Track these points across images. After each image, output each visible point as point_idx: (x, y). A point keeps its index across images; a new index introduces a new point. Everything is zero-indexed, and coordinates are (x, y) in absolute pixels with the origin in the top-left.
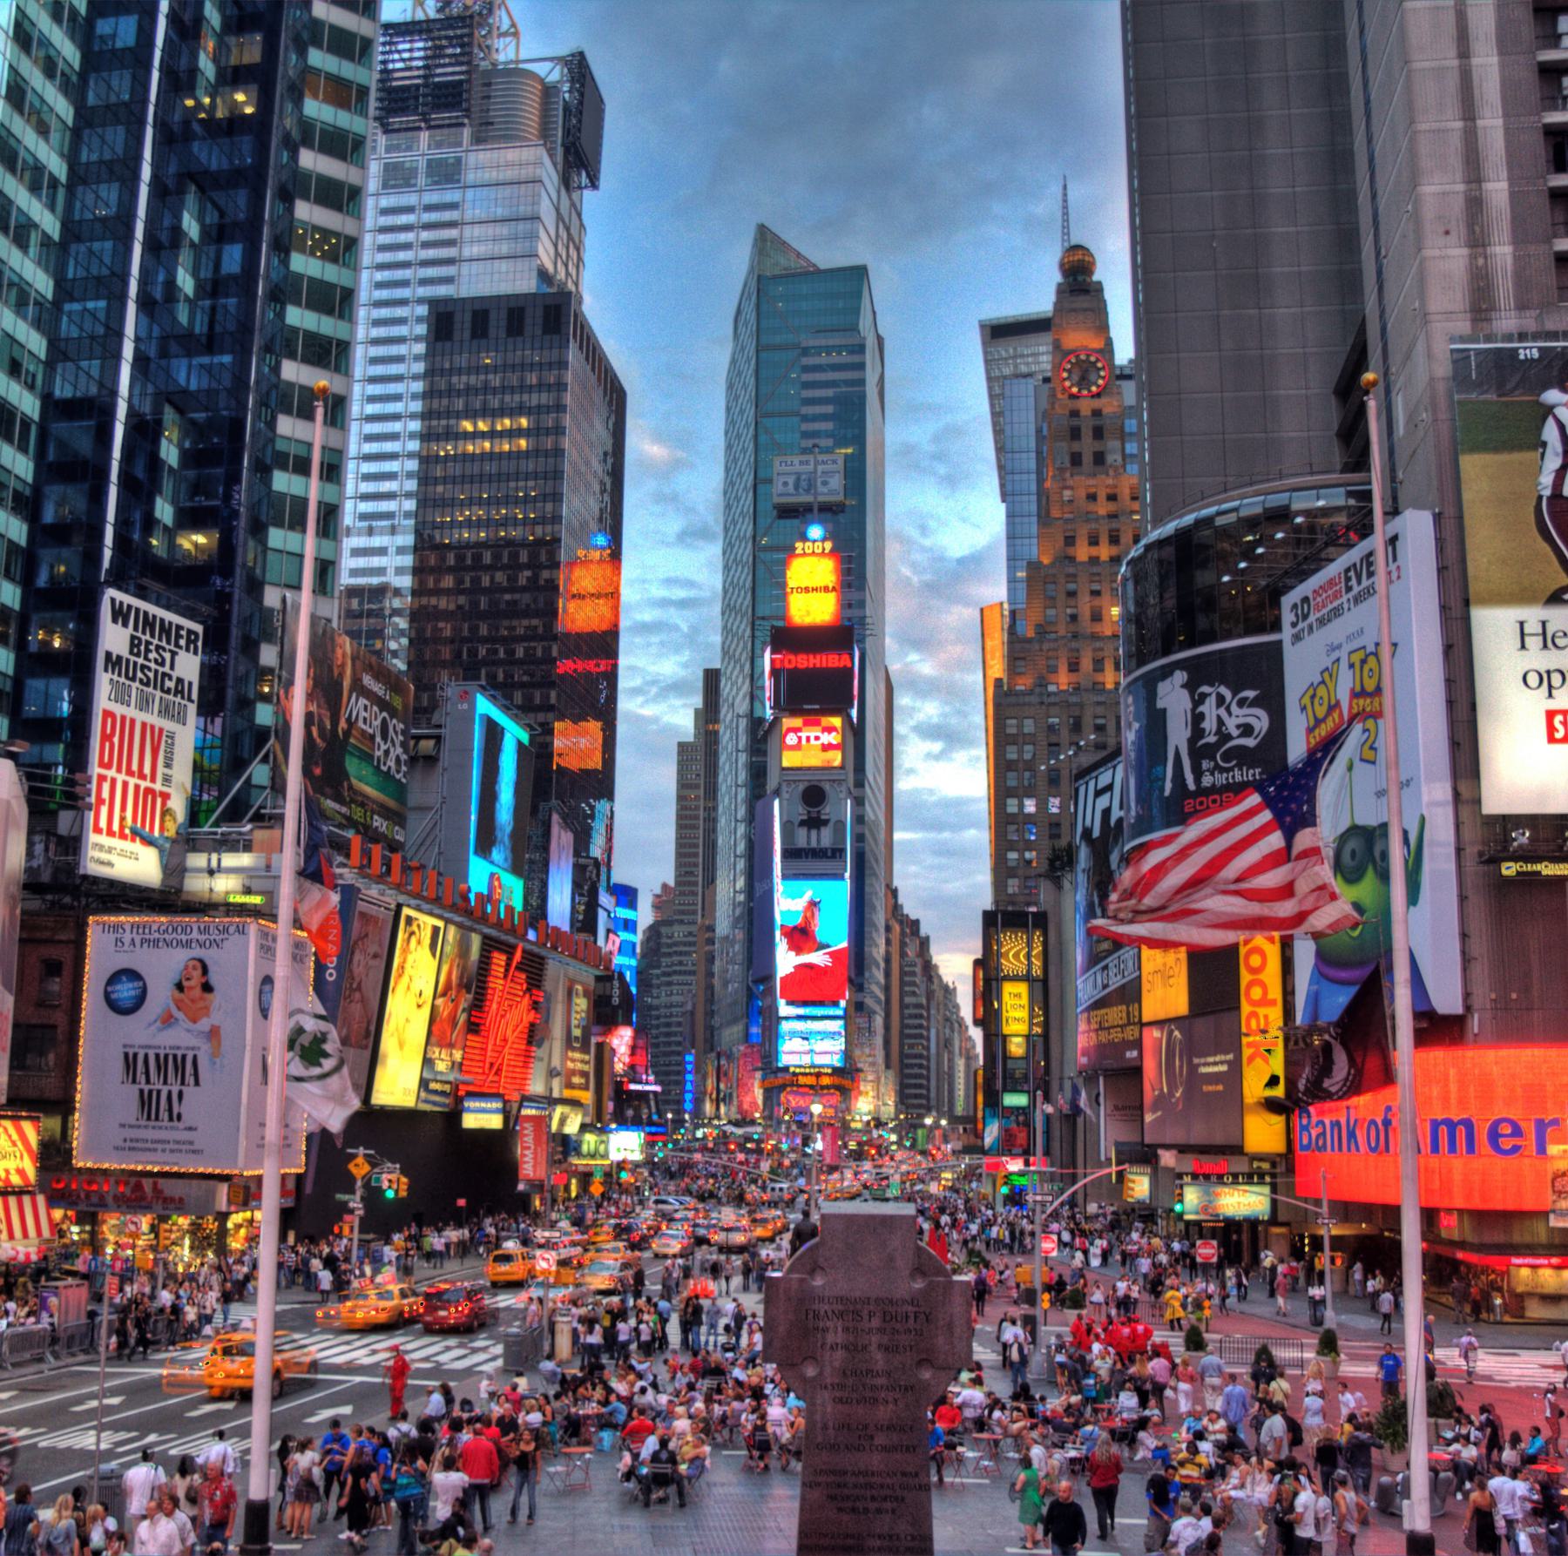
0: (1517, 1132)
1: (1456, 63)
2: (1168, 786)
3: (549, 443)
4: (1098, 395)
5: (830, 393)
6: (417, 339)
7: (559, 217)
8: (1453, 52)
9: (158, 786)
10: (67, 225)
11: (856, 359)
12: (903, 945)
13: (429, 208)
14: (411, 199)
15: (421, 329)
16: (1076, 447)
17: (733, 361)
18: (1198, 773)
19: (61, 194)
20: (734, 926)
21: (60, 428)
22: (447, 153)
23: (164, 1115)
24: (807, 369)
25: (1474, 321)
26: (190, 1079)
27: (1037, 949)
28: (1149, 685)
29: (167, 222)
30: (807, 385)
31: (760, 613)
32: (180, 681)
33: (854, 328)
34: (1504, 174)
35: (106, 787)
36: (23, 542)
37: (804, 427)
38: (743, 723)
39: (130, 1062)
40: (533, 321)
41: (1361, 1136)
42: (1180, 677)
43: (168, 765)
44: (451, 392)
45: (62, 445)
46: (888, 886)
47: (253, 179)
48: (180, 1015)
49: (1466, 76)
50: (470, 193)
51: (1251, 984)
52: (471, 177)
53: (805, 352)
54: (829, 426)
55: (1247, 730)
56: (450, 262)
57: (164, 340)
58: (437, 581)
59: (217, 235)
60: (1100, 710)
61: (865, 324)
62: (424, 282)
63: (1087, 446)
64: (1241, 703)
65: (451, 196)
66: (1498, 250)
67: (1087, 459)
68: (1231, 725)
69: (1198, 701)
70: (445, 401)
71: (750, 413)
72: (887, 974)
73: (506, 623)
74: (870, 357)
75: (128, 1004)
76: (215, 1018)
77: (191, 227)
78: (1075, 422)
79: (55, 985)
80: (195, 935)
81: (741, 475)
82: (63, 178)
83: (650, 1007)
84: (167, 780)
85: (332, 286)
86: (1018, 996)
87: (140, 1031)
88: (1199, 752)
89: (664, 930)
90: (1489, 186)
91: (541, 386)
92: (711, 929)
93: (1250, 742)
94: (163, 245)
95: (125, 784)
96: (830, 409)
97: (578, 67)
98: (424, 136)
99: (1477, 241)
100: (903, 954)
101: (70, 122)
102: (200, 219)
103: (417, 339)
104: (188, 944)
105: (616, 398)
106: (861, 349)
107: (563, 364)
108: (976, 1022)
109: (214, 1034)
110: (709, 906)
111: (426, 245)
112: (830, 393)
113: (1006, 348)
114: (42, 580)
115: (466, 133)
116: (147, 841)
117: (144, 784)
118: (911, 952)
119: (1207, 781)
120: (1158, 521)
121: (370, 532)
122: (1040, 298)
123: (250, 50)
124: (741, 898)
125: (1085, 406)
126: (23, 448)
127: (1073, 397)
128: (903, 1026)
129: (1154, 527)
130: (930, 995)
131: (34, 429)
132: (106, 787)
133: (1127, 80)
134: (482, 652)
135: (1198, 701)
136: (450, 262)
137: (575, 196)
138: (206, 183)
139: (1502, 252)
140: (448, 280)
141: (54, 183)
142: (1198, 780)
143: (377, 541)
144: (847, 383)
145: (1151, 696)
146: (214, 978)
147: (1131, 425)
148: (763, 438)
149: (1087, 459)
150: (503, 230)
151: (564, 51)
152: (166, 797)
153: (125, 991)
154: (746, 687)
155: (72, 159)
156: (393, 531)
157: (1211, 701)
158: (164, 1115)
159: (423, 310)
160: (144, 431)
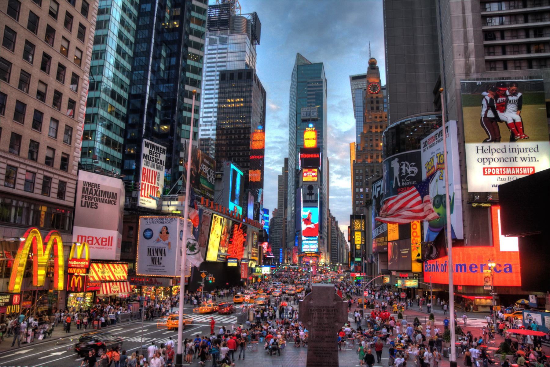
0: (476, 267)
1: (462, 15)
2: (394, 185)
3: (248, 104)
5: (314, 93)
6: (217, 80)
8: (461, 12)
9: (156, 185)
11: (320, 85)
12: (331, 223)
13: (220, 49)
14: (216, 47)
15: (218, 78)
16: (372, 105)
17: (291, 85)
18: (401, 182)
19: (133, 45)
21: (133, 101)
23: (157, 263)
24: (309, 87)
25: (466, 76)
26: (163, 255)
27: (363, 224)
28: (389, 162)
29: (158, 52)
30: (309, 91)
32: (161, 161)
33: (320, 77)
34: (474, 56)
35: (144, 186)
37: (308, 101)
38: (294, 170)
39: (149, 251)
40: (244, 76)
42: (397, 160)
43: (158, 181)
46: (328, 209)
47: (178, 42)
48: (161, 239)
49: (464, 18)
50: (229, 46)
51: (413, 232)
52: (230, 42)
53: (308, 83)
55: (412, 172)
56: (225, 62)
57: (157, 80)
59: (170, 55)
60: (378, 168)
61: (322, 76)
62: (218, 67)
63: (375, 105)
64: (411, 166)
66: (472, 59)
67: (375, 108)
68: (409, 171)
69: (401, 165)
71: (295, 97)
72: (328, 230)
74: (324, 84)
75: (149, 237)
76: (169, 240)
77: (164, 53)
78: (372, 100)
79: (132, 232)
80: (165, 221)
82: (134, 42)
83: (272, 238)
84: (158, 184)
85: (197, 68)
87: (151, 243)
88: (401, 177)
89: (275, 219)
90: (470, 44)
91: (246, 91)
92: (286, 219)
93: (413, 175)
94: (157, 58)
95: (148, 185)
96: (314, 96)
97: (255, 16)
98: (219, 32)
99: (467, 57)
100: (331, 225)
102: (166, 52)
104: (163, 223)
106: (322, 82)
107: (251, 86)
108: (349, 241)
109: (169, 244)
110: (286, 213)
112: (314, 93)
113: (356, 82)
115: (229, 31)
116: (154, 199)
117: (152, 185)
118: (333, 225)
119: (403, 184)
120: (391, 123)
121: (206, 125)
124: (293, 212)
126: (124, 106)
127: (372, 94)
128: (332, 242)
130: (338, 235)
132: (144, 186)
134: (232, 154)
135: (401, 165)
136: (225, 62)
138: (167, 43)
139: (473, 59)
140: (224, 66)
141: (131, 43)
142: (401, 184)
143: (207, 128)
144: (318, 90)
145: (390, 164)
146: (169, 231)
147: (385, 100)
148: (298, 103)
149: (375, 108)
150: (237, 54)
151: (251, 12)
152: (158, 188)
153: (148, 234)
154: (294, 162)
156: (211, 125)
157: (404, 165)
158: (157, 263)
159: (218, 73)
160: (152, 102)
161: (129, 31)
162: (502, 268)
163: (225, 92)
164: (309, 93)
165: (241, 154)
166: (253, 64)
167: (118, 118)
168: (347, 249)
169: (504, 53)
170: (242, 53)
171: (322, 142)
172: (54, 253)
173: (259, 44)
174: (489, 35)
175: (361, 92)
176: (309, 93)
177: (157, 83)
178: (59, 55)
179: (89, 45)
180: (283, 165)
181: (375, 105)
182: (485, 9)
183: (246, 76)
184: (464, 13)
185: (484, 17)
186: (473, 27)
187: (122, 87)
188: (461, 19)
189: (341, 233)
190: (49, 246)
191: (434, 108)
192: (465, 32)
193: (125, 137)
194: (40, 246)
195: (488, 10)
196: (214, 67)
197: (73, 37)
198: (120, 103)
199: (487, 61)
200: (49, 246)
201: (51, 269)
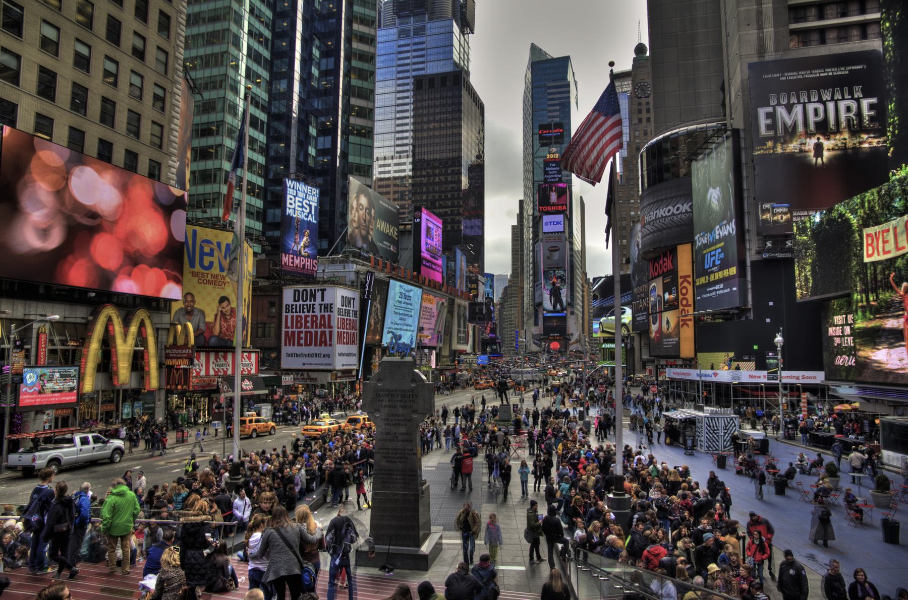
5: (558, 102)
7: (460, 44)
10: (273, 54)
13: (415, 44)
16: (640, 116)
19: (270, 43)
21: (276, 124)
22: (419, 24)
24: (550, 94)
31: (536, 179)
38: (531, 218)
45: (276, 130)
50: (429, 38)
51: (683, 299)
52: (428, 32)
53: (549, 88)
61: (570, 78)
62: (414, 70)
63: (644, 116)
67: (644, 120)
71: (530, 110)
96: (558, 108)
98: (412, 19)
105: (481, 107)
106: (568, 86)
111: (415, 57)
112: (558, 102)
114: (271, 176)
121: (400, 157)
126: (262, 131)
127: (639, 98)
137: (466, 36)
139: (769, 30)
140: (423, 69)
141: (267, 40)
143: (402, 161)
144: (563, 98)
149: (644, 120)
150: (441, 50)
156: (408, 157)
160: (303, 123)
165: (449, 196)
169: (821, 17)
170: (447, 49)
172: (141, 339)
173: (473, 33)
176: (549, 103)
177: (308, 97)
178: (131, 60)
179: (178, 42)
180: (518, 212)
181: (644, 116)
183: (456, 81)
187: (257, 105)
190: (133, 329)
194: (118, 328)
196: (408, 71)
197: (152, 31)
199: (793, 32)
200: (133, 329)
201: (138, 362)
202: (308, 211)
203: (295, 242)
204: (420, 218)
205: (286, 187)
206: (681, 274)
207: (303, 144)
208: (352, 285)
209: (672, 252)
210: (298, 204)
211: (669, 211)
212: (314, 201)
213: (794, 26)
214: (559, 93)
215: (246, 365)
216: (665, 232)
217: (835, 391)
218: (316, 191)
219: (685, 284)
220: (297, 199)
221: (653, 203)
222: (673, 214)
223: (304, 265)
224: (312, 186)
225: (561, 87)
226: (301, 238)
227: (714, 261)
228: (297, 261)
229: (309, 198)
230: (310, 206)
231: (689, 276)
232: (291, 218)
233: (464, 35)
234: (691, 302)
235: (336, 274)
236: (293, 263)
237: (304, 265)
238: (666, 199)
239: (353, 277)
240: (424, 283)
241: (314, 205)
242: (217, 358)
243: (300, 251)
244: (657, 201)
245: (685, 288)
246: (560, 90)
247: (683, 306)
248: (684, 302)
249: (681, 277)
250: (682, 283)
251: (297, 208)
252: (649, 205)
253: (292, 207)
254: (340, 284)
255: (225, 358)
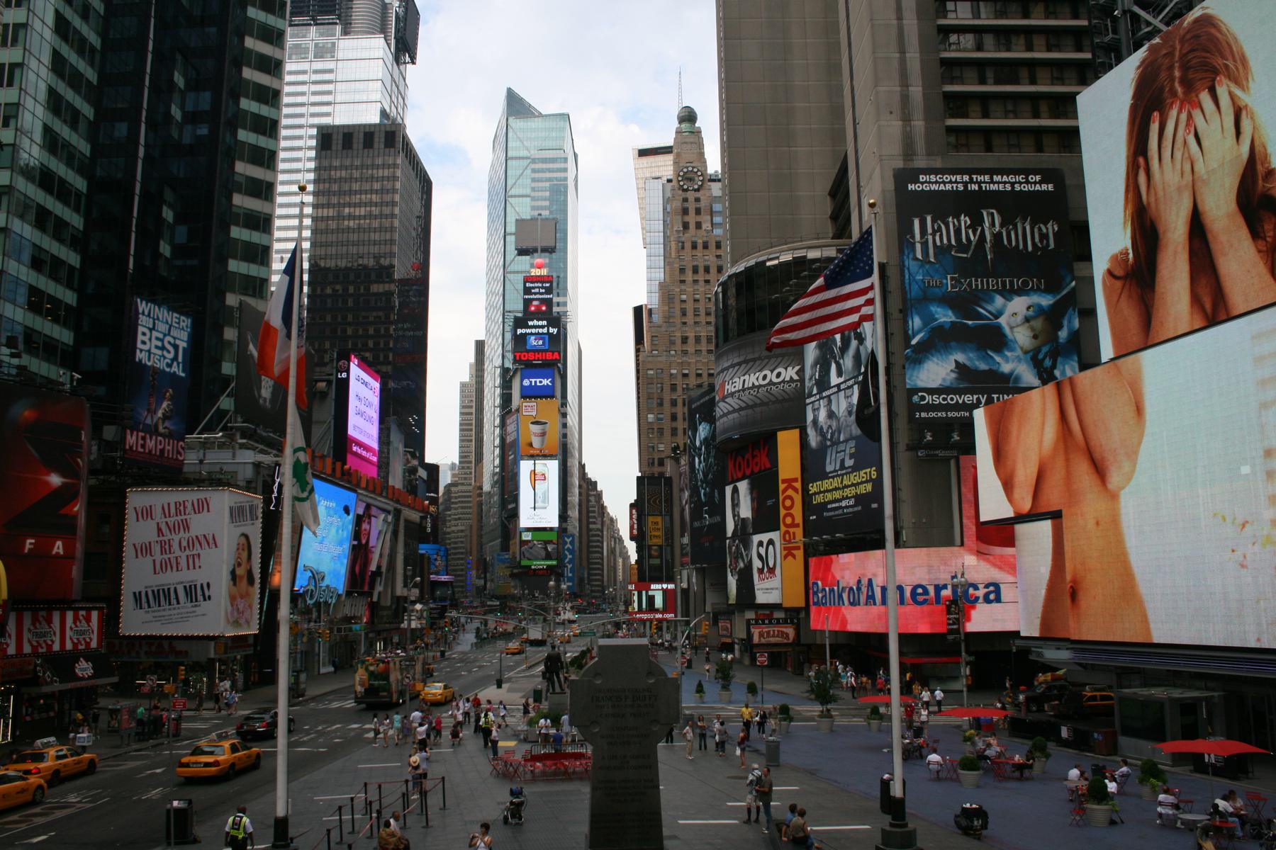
0: (926, 592)
1: (895, 22)
4: (698, 190)
5: (547, 184)
6: (310, 148)
8: (894, 16)
13: (316, 72)
14: (305, 66)
15: (313, 143)
16: (674, 425)
17: (492, 165)
19: (98, 57)
20: (492, 487)
22: (322, 40)
23: (200, 598)
24: (534, 171)
30: (534, 180)
31: (507, 308)
34: (921, 116)
36: (75, 304)
40: (379, 142)
41: (845, 596)
44: (331, 180)
46: (580, 462)
49: (901, 29)
51: (786, 516)
52: (340, 55)
54: (547, 203)
56: (328, 104)
58: (322, 290)
59: (194, 85)
63: (692, 219)
65: (331, 65)
66: (916, 123)
67: (692, 226)
70: (327, 185)
73: (363, 314)
74: (571, 164)
77: (179, 80)
79: (107, 529)
81: (496, 230)
82: (99, 47)
86: (656, 523)
89: (453, 489)
98: (313, 29)
99: (906, 119)
101: (102, 13)
102: (185, 76)
103: (310, 148)
106: (566, 160)
108: (632, 538)
110: (479, 475)
120: (734, 262)
122: (668, 139)
123: (205, 100)
124: (497, 470)
125: (691, 196)
126: (77, 210)
129: (732, 266)
130: (603, 523)
131: (77, 274)
133: (718, 19)
134: (349, 332)
136: (328, 104)
137: (402, 67)
139: (919, 124)
140: (328, 114)
141: (78, 194)
147: (717, 207)
149: (692, 226)
155: (103, 35)
158: (200, 598)
159: (314, 132)
160: (152, 201)
161: (74, 125)
162: (981, 593)
163: (331, 180)
164: (534, 185)
166: (400, 110)
167: (61, 241)
168: (626, 558)
171: (565, 304)
173: (413, 63)
174: (951, 68)
175: (658, 185)
180: (473, 360)
181: (692, 219)
182: (943, 13)
183: (387, 138)
184: (900, 18)
185: (945, 31)
186: (921, 52)
188: (894, 32)
189: (612, 520)
191: (830, 229)
192: (903, 62)
193: (80, 291)
195: (951, 15)
198: (66, 203)
202: (171, 356)
203: (149, 411)
204: (348, 371)
205: (137, 312)
206: (782, 476)
207: (149, 238)
208: (249, 486)
209: (768, 442)
210: (155, 342)
211: (765, 377)
212: (182, 338)
213: (952, 122)
214: (550, 171)
215: (83, 633)
216: (758, 410)
217: (1040, 655)
218: (186, 322)
219: (790, 492)
220: (155, 334)
221: (739, 364)
222: (771, 383)
223: (162, 451)
224: (181, 313)
225: (553, 160)
226: (159, 404)
227: (843, 461)
228: (151, 444)
229: (174, 333)
230: (176, 347)
231: (795, 480)
232: (142, 367)
233: (398, 64)
234: (799, 519)
235: (225, 468)
236: (143, 446)
237: (162, 451)
238: (759, 358)
239: (249, 473)
240: (358, 485)
241: (182, 345)
242: (35, 621)
243: (156, 426)
244: (746, 362)
245: (790, 497)
246: (551, 166)
247: (786, 525)
248: (789, 520)
249: (784, 481)
250: (784, 491)
251: (154, 350)
252: (733, 366)
253: (146, 347)
254: (229, 485)
255: (49, 621)
